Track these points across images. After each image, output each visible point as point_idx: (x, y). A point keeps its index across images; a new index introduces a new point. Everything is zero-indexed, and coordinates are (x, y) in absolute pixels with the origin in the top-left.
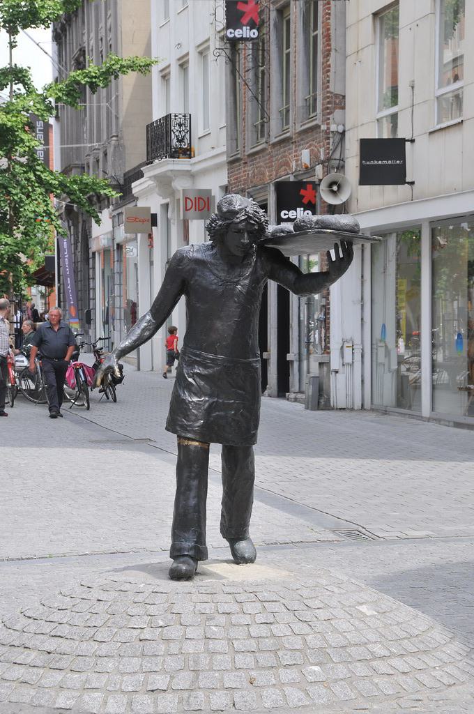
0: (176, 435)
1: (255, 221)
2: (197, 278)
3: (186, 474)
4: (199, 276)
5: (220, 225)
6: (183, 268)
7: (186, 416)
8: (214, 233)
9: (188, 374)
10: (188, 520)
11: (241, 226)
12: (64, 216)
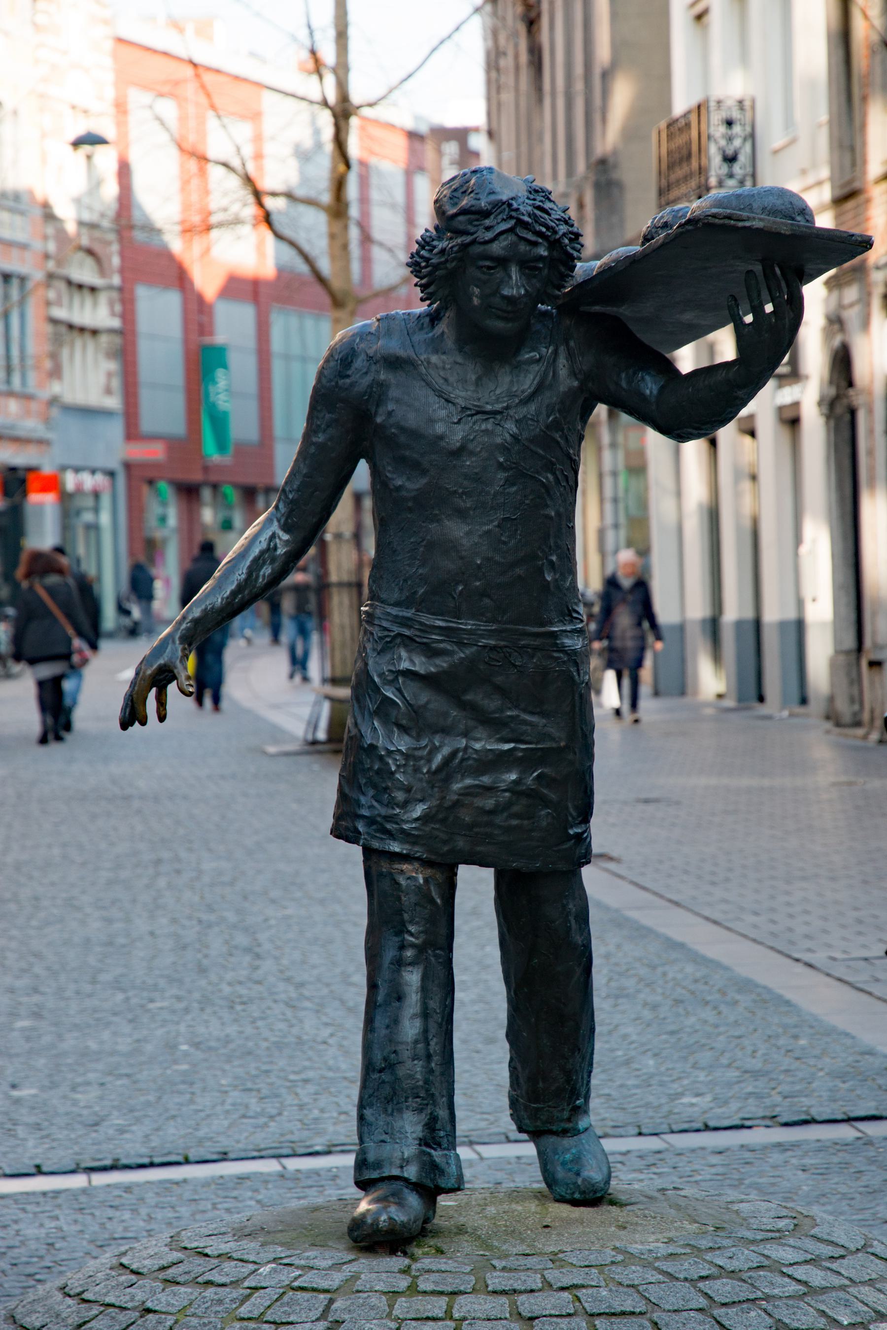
0: (356, 851)
1: (540, 234)
2: (391, 406)
3: (389, 954)
4: (398, 401)
5: (443, 251)
6: (352, 385)
7: (381, 792)
8: (429, 274)
9: (381, 675)
10: (403, 1079)
11: (497, 248)
12: (450, 343)
